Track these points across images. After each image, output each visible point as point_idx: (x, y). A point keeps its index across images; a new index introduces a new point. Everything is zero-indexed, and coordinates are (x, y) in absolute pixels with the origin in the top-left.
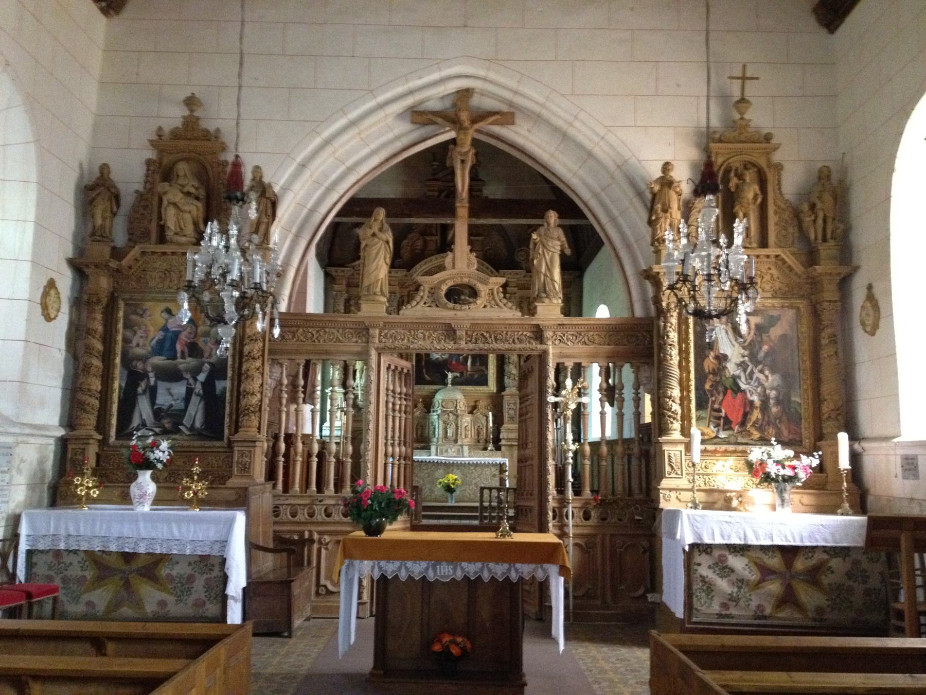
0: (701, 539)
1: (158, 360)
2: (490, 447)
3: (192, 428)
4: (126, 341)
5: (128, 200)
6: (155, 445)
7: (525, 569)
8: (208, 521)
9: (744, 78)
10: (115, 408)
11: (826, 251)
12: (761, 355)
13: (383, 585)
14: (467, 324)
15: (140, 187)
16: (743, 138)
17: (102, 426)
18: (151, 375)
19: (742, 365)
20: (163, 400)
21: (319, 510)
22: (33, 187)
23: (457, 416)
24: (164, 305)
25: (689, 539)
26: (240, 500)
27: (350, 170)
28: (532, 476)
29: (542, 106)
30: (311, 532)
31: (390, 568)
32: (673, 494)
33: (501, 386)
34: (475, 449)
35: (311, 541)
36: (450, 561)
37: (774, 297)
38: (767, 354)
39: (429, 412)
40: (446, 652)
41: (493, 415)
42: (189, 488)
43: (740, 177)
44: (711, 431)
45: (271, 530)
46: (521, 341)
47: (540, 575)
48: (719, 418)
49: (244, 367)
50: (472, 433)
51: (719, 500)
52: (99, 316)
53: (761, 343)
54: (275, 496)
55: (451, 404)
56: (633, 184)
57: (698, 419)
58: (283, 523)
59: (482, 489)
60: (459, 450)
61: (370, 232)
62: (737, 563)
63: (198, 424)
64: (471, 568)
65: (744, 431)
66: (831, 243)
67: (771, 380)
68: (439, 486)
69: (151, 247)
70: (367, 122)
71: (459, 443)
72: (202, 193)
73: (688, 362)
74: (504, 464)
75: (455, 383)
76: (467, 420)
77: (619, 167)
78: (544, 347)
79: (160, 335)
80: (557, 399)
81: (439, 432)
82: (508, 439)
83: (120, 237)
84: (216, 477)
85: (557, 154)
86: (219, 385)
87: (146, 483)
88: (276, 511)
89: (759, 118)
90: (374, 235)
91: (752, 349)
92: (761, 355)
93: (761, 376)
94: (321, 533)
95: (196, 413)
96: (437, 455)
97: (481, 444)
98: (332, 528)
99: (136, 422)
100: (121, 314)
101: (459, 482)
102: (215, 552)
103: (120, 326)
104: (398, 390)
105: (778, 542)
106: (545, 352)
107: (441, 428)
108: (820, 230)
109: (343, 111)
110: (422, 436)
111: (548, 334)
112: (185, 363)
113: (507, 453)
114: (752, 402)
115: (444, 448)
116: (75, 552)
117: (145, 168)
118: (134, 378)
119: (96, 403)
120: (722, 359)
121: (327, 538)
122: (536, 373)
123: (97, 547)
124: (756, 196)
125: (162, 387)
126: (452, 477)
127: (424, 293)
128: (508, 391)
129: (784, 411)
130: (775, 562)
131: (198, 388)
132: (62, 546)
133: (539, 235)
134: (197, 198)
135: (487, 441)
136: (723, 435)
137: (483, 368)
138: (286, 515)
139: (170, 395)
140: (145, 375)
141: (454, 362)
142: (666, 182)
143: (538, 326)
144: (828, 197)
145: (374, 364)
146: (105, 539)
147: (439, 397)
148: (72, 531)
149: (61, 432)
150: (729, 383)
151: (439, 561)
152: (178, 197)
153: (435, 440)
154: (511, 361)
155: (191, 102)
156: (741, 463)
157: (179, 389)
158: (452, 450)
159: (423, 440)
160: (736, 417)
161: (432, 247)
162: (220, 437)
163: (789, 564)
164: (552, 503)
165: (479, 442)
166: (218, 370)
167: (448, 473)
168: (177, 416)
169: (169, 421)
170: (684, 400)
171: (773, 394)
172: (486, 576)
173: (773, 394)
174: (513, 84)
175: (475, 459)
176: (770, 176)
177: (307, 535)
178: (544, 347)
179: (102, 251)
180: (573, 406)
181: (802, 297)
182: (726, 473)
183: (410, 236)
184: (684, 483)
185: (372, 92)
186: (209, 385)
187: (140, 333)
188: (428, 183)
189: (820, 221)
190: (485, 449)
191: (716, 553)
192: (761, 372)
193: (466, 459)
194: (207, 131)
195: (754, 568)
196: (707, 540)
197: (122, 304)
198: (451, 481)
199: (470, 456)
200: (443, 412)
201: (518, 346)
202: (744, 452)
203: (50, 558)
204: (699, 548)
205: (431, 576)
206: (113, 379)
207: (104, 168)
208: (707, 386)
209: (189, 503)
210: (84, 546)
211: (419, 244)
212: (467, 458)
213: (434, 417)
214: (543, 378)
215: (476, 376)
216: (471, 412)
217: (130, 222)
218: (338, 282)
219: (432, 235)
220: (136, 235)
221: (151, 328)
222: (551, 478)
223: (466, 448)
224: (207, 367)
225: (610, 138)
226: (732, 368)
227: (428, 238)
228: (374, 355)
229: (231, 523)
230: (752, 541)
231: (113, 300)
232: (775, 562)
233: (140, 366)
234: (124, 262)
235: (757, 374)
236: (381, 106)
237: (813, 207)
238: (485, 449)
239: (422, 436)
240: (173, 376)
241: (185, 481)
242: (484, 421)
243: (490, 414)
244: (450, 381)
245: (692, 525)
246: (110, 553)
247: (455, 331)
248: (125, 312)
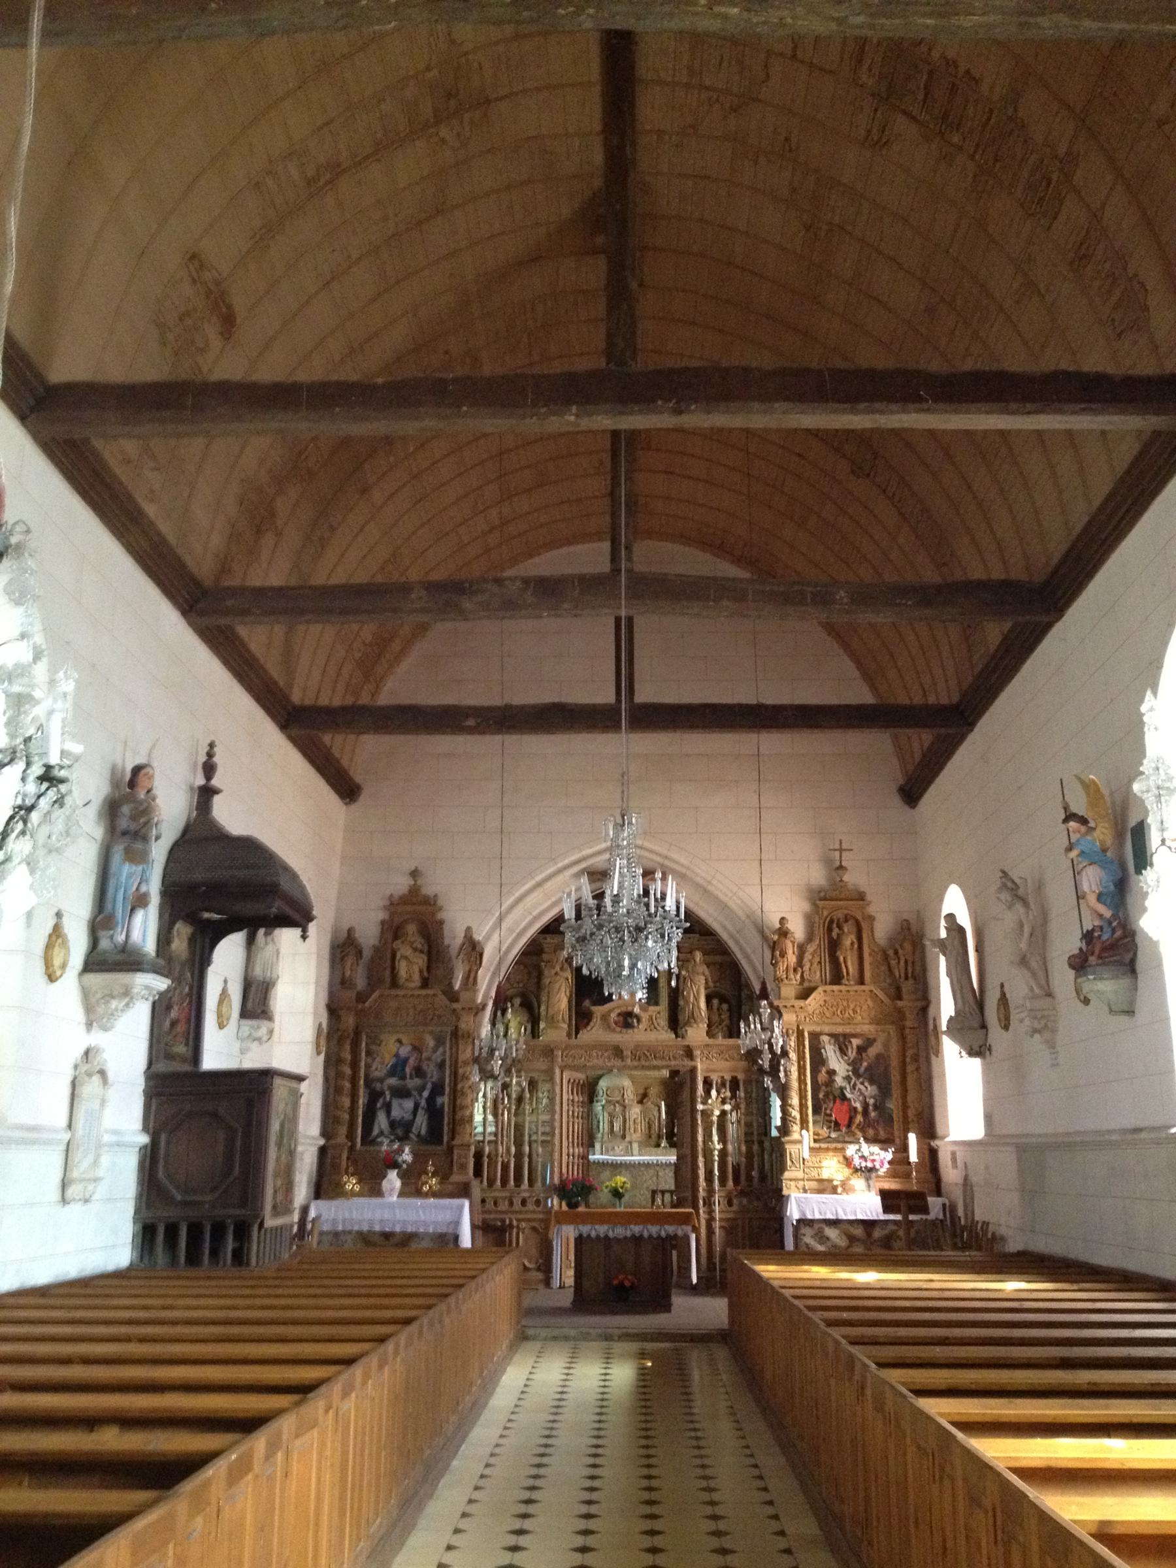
0: (804, 1214)
1: (393, 1081)
3: (419, 1136)
4: (368, 1066)
5: (367, 953)
6: (400, 1151)
7: (670, 1229)
8: (444, 1208)
9: (841, 850)
10: (360, 1120)
11: (907, 987)
12: (862, 1070)
13: (580, 1240)
14: (632, 1046)
15: (377, 943)
16: (843, 896)
17: (351, 1136)
18: (387, 1093)
19: (848, 1078)
20: (396, 1113)
21: (517, 1202)
22: (314, 957)
24: (395, 1037)
25: (796, 1216)
26: (463, 1191)
27: (536, 918)
28: (686, 1169)
29: (688, 868)
30: (511, 1220)
31: (585, 1229)
32: (793, 1183)
34: (646, 1146)
35: (511, 1226)
36: (622, 1225)
37: (870, 1023)
38: (866, 1069)
40: (622, 1284)
42: (426, 1183)
43: (840, 927)
44: (824, 1132)
45: (481, 1217)
46: (675, 1058)
47: (680, 1233)
48: (830, 1122)
49: (459, 1086)
50: (642, 1127)
51: (826, 1187)
52: (348, 1047)
53: (862, 1059)
54: (482, 1190)
56: (761, 932)
57: (815, 1122)
58: (490, 1212)
59: (654, 1193)
61: (553, 972)
62: (832, 1233)
63: (423, 1132)
64: (636, 1229)
65: (850, 1133)
66: (911, 981)
67: (870, 1090)
69: (386, 992)
70: (549, 884)
71: (628, 1139)
72: (426, 949)
73: (805, 1075)
76: (635, 1111)
77: (748, 917)
78: (693, 1063)
79: (393, 1061)
80: (706, 1107)
81: (604, 1126)
83: (361, 983)
84: (444, 1175)
85: (701, 903)
86: (439, 1100)
87: (393, 1181)
88: (483, 1201)
89: (855, 878)
90: (556, 974)
91: (855, 1065)
92: (862, 1070)
93: (862, 1087)
94: (518, 1220)
95: (421, 1123)
97: (652, 1140)
98: (529, 1216)
99: (376, 1132)
100: (364, 1045)
101: (628, 1186)
102: (451, 1231)
103: (363, 1054)
104: (576, 1099)
105: (860, 1217)
106: (693, 1071)
108: (903, 971)
109: (531, 875)
111: (697, 1053)
112: (412, 1083)
114: (855, 1109)
115: (610, 1146)
116: (350, 1232)
117: (379, 928)
118: (374, 1096)
119: (346, 1116)
120: (832, 1073)
121: (523, 1224)
122: (688, 1084)
123: (365, 1228)
124: (852, 944)
125: (395, 1103)
126: (620, 1179)
127: (596, 1020)
129: (880, 1116)
130: (859, 1232)
131: (423, 1103)
132: (340, 1228)
133: (688, 971)
134: (422, 952)
135: (659, 1137)
136: (833, 1135)
138: (490, 1205)
139: (402, 1109)
140: (382, 1093)
142: (783, 933)
143: (688, 1046)
144: (908, 946)
145: (558, 1080)
146: (371, 1222)
148: (347, 1216)
149: (322, 1142)
150: (837, 1093)
151: (615, 1224)
152: (407, 951)
153: (599, 1135)
155: (415, 874)
156: (841, 1159)
157: (409, 1104)
158: (620, 1147)
159: (589, 1141)
160: (844, 1121)
162: (440, 1143)
163: (869, 1235)
164: (702, 1193)
166: (438, 1090)
168: (408, 1126)
169: (400, 1131)
170: (803, 1106)
171: (871, 1101)
172: (646, 1234)
173: (871, 1101)
174: (664, 852)
175: (646, 1158)
176: (864, 925)
177: (507, 1222)
178: (693, 1063)
179: (351, 995)
180: (717, 1113)
181: (893, 1023)
182: (832, 1167)
184: (800, 1175)
185: (553, 860)
186: (431, 1100)
187: (378, 1059)
189: (902, 962)
190: (658, 1145)
191: (816, 1226)
192: (862, 1083)
194: (428, 897)
195: (844, 1237)
196: (809, 1217)
197: (364, 1037)
199: (640, 1155)
200: (608, 1102)
201: (673, 1063)
202: (843, 1149)
203: (330, 1237)
204: (803, 1222)
205: (611, 1234)
206: (358, 1097)
207: (350, 931)
208: (821, 1096)
209: (426, 1195)
210: (356, 1228)
213: (598, 1107)
214: (694, 1089)
216: (641, 1102)
217: (369, 970)
220: (374, 982)
221: (387, 1055)
222: (701, 1173)
223: (635, 1146)
224: (429, 1086)
225: (741, 893)
226: (839, 1081)
228: (558, 1071)
229: (461, 1208)
230: (843, 1217)
231: (357, 1033)
232: (859, 1232)
233: (378, 1086)
234: (367, 1004)
235: (859, 1086)
236: (560, 871)
237: (896, 953)
238: (658, 1145)
240: (402, 1093)
241: (424, 1178)
245: (799, 1206)
246: (374, 1233)
247: (622, 1051)
248: (367, 1044)
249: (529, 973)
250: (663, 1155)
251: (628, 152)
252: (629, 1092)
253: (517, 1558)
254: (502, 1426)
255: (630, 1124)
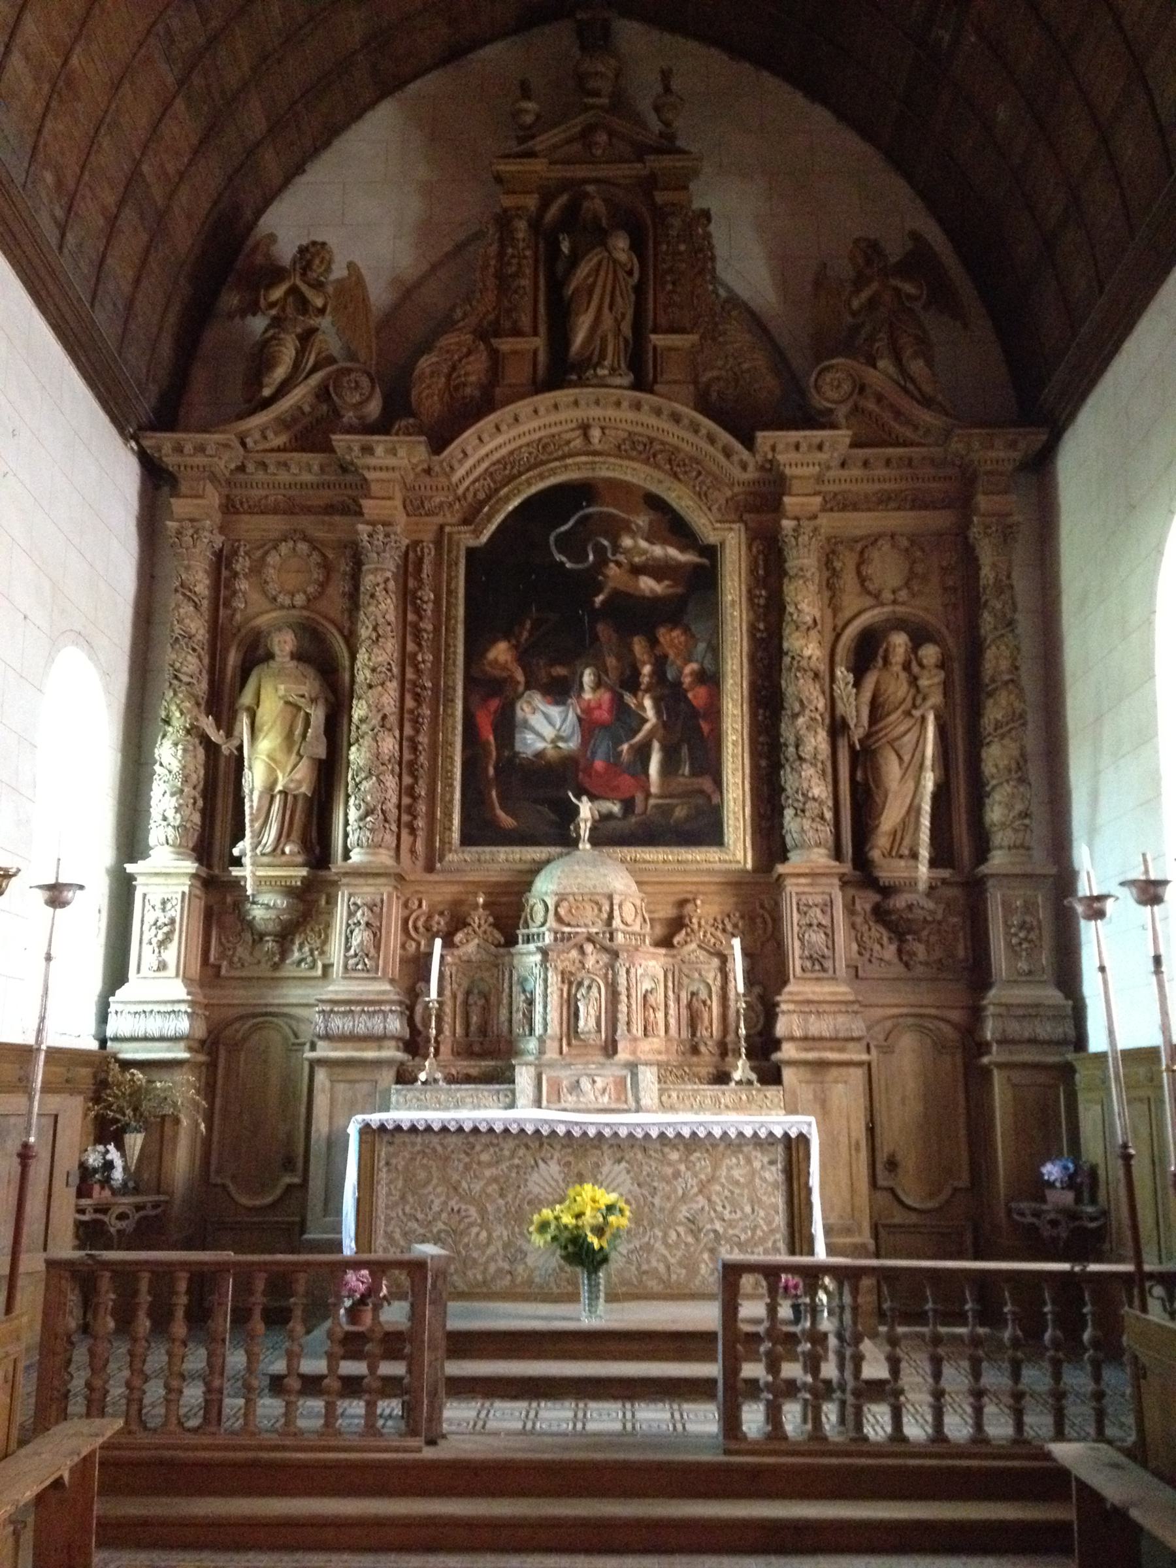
2: (741, 1069)
23: (615, 955)
33: (771, 843)
39: (511, 941)
41: (746, 953)
50: (668, 1018)
55: (589, 912)
60: (621, 1083)
68: (538, 1240)
71: (623, 1055)
74: (803, 1139)
75: (600, 839)
76: (649, 969)
81: (548, 1015)
82: (807, 1040)
96: (538, 1103)
107: (554, 1000)
110: (483, 1031)
113: (806, 1093)
115: (565, 1076)
126: (592, 1198)
128: (797, 861)
135: (724, 1050)
137: (706, 784)
141: (599, 764)
147: (545, 887)
154: (807, 750)
158: (597, 1085)
161: (518, 373)
165: (695, 1050)
167: (581, 1179)
175: (686, 1120)
183: (443, 342)
188: (504, 167)
193: (651, 1118)
198: (589, 1219)
199: (663, 1107)
200: (561, 938)
211: (475, 369)
212: (654, 1113)
213: (528, 958)
215: (680, 813)
216: (666, 942)
218: (184, 488)
219: (517, 332)
223: (648, 1077)
227: (505, 345)
238: (722, 1078)
239: (483, 1031)
242: (712, 975)
243: (736, 943)
244: (585, 830)
249: (327, 567)
250: (737, 1107)
251: (403, 423)
252: (629, 911)
253: (24, 894)
254: (72, 1208)
255: (630, 1010)
